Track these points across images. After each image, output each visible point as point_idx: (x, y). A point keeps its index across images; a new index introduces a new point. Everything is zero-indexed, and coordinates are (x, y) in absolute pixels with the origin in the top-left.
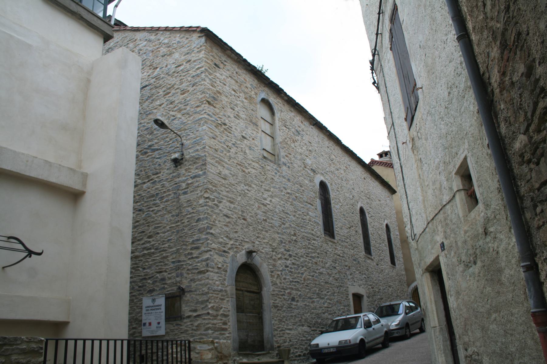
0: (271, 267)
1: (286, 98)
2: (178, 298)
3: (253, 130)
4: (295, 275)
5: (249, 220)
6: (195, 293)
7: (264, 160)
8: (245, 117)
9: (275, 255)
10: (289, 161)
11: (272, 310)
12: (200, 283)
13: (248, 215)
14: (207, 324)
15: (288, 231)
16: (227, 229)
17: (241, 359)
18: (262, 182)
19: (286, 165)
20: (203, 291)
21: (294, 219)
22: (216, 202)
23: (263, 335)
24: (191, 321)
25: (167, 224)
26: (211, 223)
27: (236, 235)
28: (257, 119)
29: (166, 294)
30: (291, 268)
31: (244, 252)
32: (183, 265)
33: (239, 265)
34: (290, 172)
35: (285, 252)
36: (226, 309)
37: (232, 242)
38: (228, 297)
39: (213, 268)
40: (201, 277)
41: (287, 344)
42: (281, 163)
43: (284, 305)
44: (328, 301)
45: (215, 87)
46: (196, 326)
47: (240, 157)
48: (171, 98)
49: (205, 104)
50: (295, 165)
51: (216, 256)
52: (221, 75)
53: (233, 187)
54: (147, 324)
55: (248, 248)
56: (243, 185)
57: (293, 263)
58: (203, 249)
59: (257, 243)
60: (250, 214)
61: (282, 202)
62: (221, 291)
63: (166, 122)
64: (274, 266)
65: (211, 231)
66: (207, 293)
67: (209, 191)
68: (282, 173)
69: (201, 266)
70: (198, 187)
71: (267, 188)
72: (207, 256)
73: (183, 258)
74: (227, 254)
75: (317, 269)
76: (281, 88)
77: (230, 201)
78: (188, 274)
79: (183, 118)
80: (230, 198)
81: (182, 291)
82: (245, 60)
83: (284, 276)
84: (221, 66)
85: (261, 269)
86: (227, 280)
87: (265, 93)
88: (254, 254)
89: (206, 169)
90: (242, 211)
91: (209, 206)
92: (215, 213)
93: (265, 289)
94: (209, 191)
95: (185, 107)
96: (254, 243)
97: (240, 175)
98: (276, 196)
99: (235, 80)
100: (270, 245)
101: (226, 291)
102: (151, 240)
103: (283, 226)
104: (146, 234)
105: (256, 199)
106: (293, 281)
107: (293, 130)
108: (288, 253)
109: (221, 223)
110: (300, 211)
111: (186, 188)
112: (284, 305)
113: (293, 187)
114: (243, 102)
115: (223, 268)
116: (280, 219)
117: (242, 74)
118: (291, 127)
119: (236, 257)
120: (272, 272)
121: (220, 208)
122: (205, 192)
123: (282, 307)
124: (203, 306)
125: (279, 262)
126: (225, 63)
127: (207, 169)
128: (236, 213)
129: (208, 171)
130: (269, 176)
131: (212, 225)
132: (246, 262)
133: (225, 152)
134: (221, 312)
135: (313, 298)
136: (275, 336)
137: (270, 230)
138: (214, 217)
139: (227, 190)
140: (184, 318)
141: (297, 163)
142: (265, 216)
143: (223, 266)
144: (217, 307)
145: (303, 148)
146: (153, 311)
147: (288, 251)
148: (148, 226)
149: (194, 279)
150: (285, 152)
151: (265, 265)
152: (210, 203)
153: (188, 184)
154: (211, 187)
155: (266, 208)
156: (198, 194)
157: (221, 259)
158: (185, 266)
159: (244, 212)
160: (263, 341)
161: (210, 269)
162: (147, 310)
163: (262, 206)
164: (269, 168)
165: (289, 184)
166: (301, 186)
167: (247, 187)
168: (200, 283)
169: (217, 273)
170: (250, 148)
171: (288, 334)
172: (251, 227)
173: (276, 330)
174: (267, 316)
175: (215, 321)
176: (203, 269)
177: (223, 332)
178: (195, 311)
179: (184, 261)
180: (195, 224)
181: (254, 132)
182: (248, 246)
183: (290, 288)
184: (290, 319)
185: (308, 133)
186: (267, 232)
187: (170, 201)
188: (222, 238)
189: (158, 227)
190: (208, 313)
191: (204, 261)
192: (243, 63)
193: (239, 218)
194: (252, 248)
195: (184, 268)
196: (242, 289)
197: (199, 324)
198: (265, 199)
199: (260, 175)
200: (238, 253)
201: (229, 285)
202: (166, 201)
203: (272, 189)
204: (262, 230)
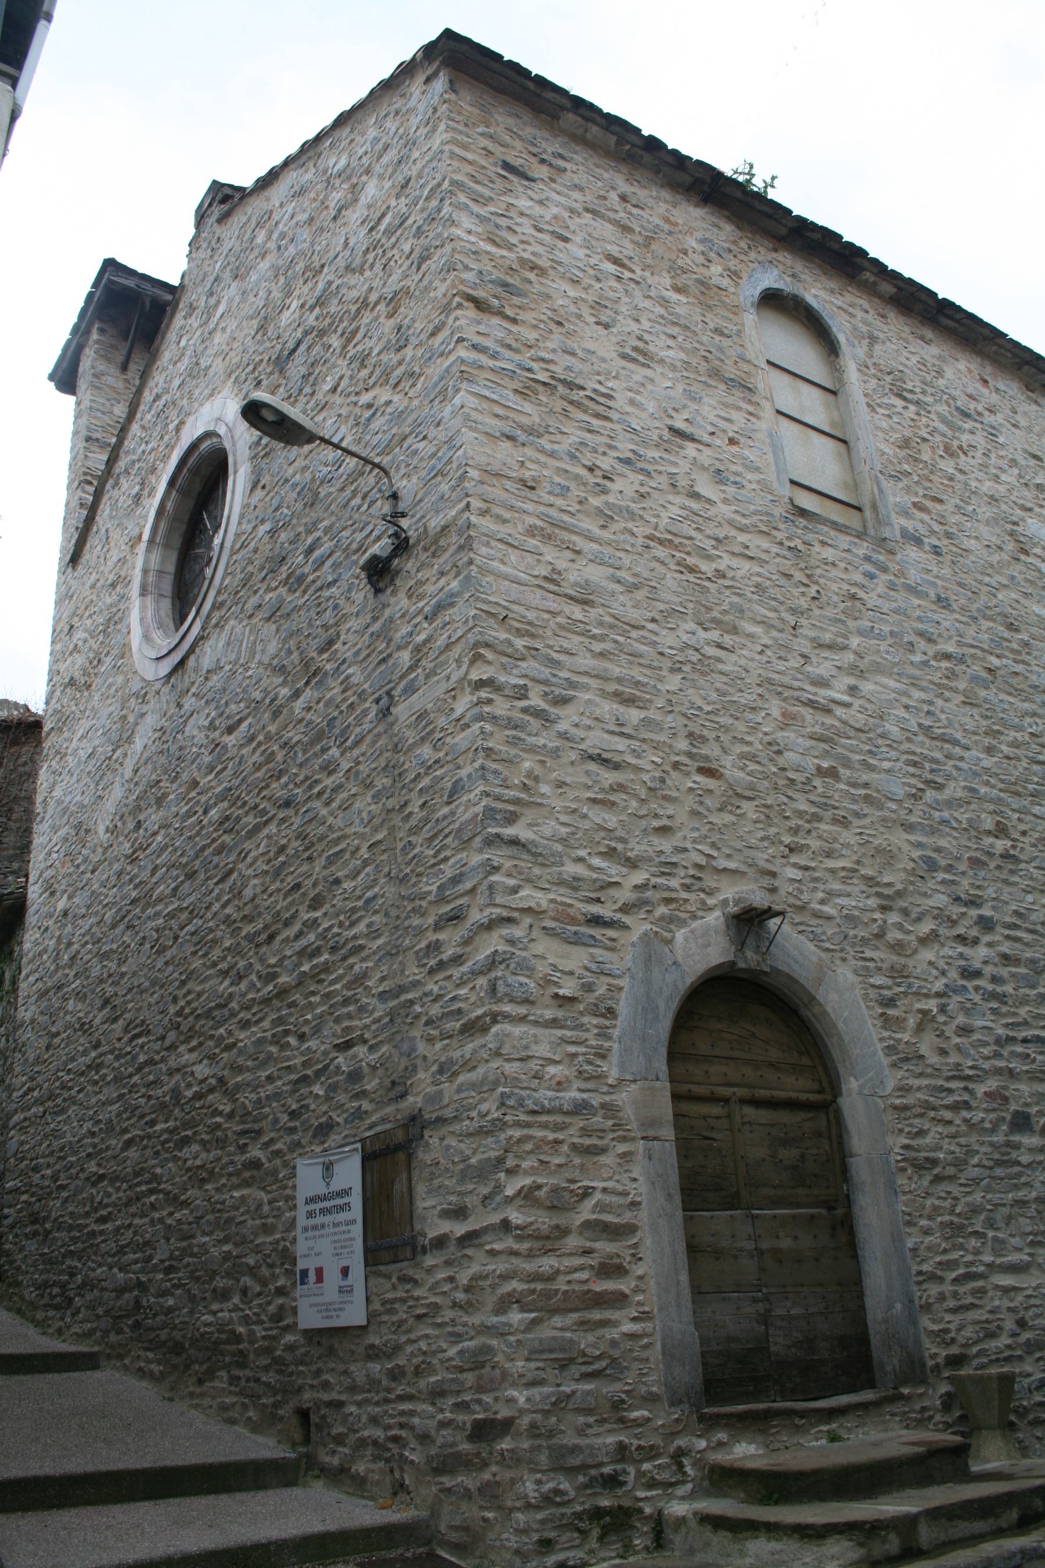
0: (878, 980)
1: (887, 288)
2: (401, 1156)
3: (726, 405)
4: (1023, 1011)
5: (732, 771)
6: (456, 1127)
7: (802, 522)
8: (682, 356)
9: (900, 927)
10: (936, 527)
11: (901, 1181)
12: (472, 1076)
13: (725, 751)
14: (505, 1277)
15: (964, 816)
16: (611, 820)
17: (721, 1444)
18: (793, 611)
19: (918, 541)
20: (483, 1116)
21: (988, 762)
22: (535, 700)
23: (862, 1308)
24: (448, 1263)
25: (362, 836)
26: (512, 793)
27: (666, 845)
28: (746, 367)
29: (362, 1141)
30: (995, 979)
31: (714, 919)
32: (411, 1002)
33: (689, 980)
34: (946, 571)
35: (956, 910)
36: (608, 1199)
37: (639, 877)
38: (624, 1139)
39: (527, 1001)
40: (474, 1052)
41: (1004, 1340)
42: (892, 532)
43: (970, 1152)
45: (511, 247)
46: (468, 1289)
47: (670, 510)
48: (360, 348)
49: (459, 306)
50: (972, 544)
51: (542, 945)
52: (541, 202)
53: (634, 634)
54: (312, 1276)
55: (737, 902)
56: (691, 626)
57: (1005, 957)
58: (476, 916)
59: (792, 873)
60: (739, 749)
61: (917, 694)
62: (580, 1108)
63: (293, 412)
64: (898, 973)
65: (509, 831)
66: (500, 1125)
67: (489, 655)
68: (901, 574)
69: (473, 999)
70: (448, 647)
71: (827, 637)
72: (493, 943)
73: (413, 972)
74: (611, 933)
76: (850, 245)
77: (616, 694)
78: (431, 1040)
79: (396, 398)
80: (619, 680)
81: (415, 1126)
82: (654, 144)
83: (961, 1019)
84: (541, 172)
85: (820, 996)
86: (614, 1058)
87: (774, 270)
88: (773, 923)
89: (471, 562)
90: (691, 735)
91: (494, 719)
92: (533, 750)
93: (851, 1085)
94: (489, 655)
95: (399, 356)
96: (773, 875)
97: (669, 582)
98: (878, 669)
99: (616, 223)
100: (869, 880)
101: (609, 1109)
102: (318, 914)
103: (930, 795)
104: (304, 894)
105: (770, 681)
106: (1011, 1040)
107: (942, 408)
108: (974, 912)
109: (572, 794)
110: (1020, 729)
111: (411, 669)
112: (970, 1152)
113: (971, 631)
114: (664, 302)
115: (591, 998)
116: (915, 764)
117: (651, 202)
118: (929, 399)
119: (669, 942)
120: (890, 1002)
121: (563, 726)
122: (472, 662)
123: (960, 1164)
124: (485, 1191)
125: (928, 954)
126: (561, 163)
127: (478, 560)
128: (656, 746)
129: (484, 571)
130: (834, 587)
131: (517, 801)
132: (733, 963)
133: (576, 491)
134: (586, 1212)
136: (927, 1308)
137: (857, 815)
138: (527, 764)
139: (598, 647)
140: (424, 1251)
141: (980, 538)
142: (826, 754)
143: (588, 988)
144: (556, 1190)
145: (1004, 477)
146: (328, 1219)
147: (973, 902)
148: (310, 858)
149: (451, 1062)
150: (908, 490)
151: (845, 974)
152: (501, 707)
153: (418, 649)
154: (503, 636)
155: (829, 721)
156: (448, 678)
157: (577, 959)
158: (418, 1009)
159: (704, 740)
160: (864, 1339)
161: (507, 1008)
162: (310, 1215)
163: (806, 712)
164: (828, 553)
165: (948, 620)
166: (1011, 627)
167: (714, 635)
168: (472, 1076)
169: (554, 1023)
170: (719, 476)
171: (1007, 1290)
172: (747, 806)
173: (933, 1277)
174: (873, 1215)
175: (547, 1264)
176: (479, 1012)
177: (597, 1315)
178: (459, 1213)
179: (416, 984)
180: (446, 810)
181: (737, 416)
182: (736, 892)
183: (998, 1071)
184: (1009, 1219)
185: (1023, 423)
186: (843, 822)
187: (368, 740)
188: (580, 860)
189: (337, 854)
190: (506, 1225)
191: (481, 973)
192: (647, 158)
193: (676, 765)
194: (759, 899)
195: (417, 1017)
196: (726, 1091)
197: (474, 1278)
198: (822, 683)
199: (783, 582)
200: (682, 923)
201: (634, 1081)
202: (357, 743)
203: (855, 642)
204: (816, 818)
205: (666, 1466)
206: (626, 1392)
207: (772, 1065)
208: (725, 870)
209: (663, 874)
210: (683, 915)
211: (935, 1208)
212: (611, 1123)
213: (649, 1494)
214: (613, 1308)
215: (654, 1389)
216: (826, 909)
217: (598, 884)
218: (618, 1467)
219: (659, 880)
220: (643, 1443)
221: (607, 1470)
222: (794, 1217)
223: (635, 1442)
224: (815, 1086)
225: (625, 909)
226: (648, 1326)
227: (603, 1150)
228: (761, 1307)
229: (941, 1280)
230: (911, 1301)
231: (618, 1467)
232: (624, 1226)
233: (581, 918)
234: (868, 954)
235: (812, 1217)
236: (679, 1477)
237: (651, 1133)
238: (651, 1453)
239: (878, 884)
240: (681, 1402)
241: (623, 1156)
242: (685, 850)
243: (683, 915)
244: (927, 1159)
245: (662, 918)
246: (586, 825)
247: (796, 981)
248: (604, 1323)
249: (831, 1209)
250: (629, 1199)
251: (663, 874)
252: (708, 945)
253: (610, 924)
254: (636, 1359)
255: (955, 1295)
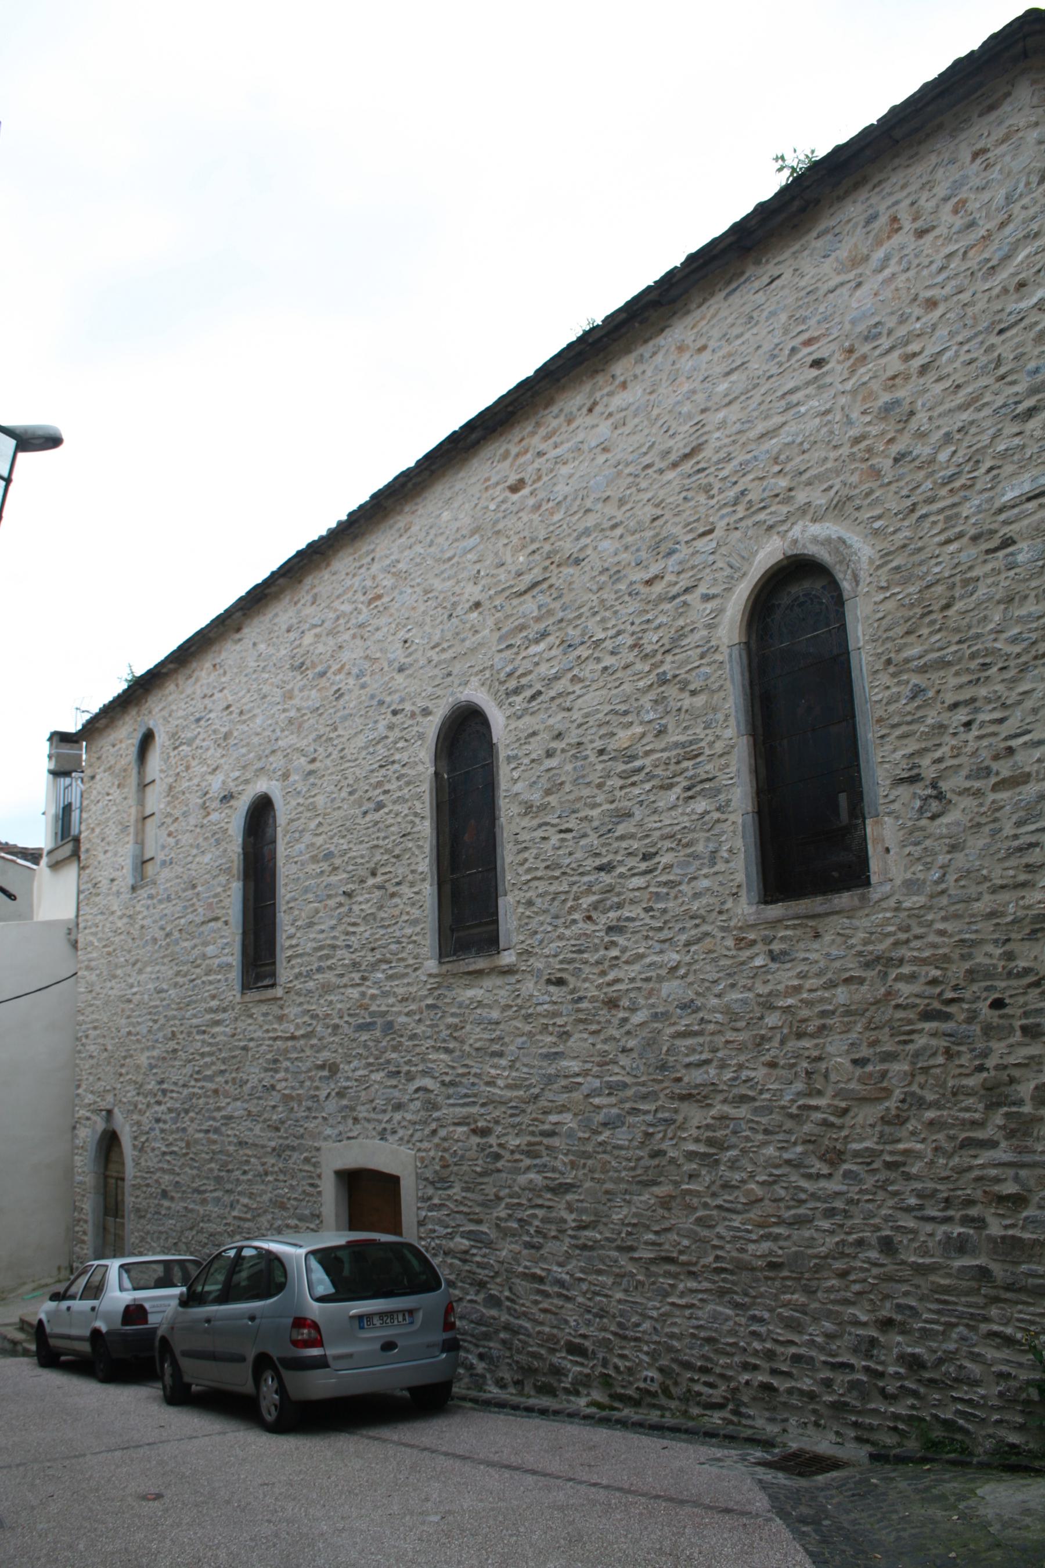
44: (245, 1200)
75: (219, 1109)
135: (205, 1191)
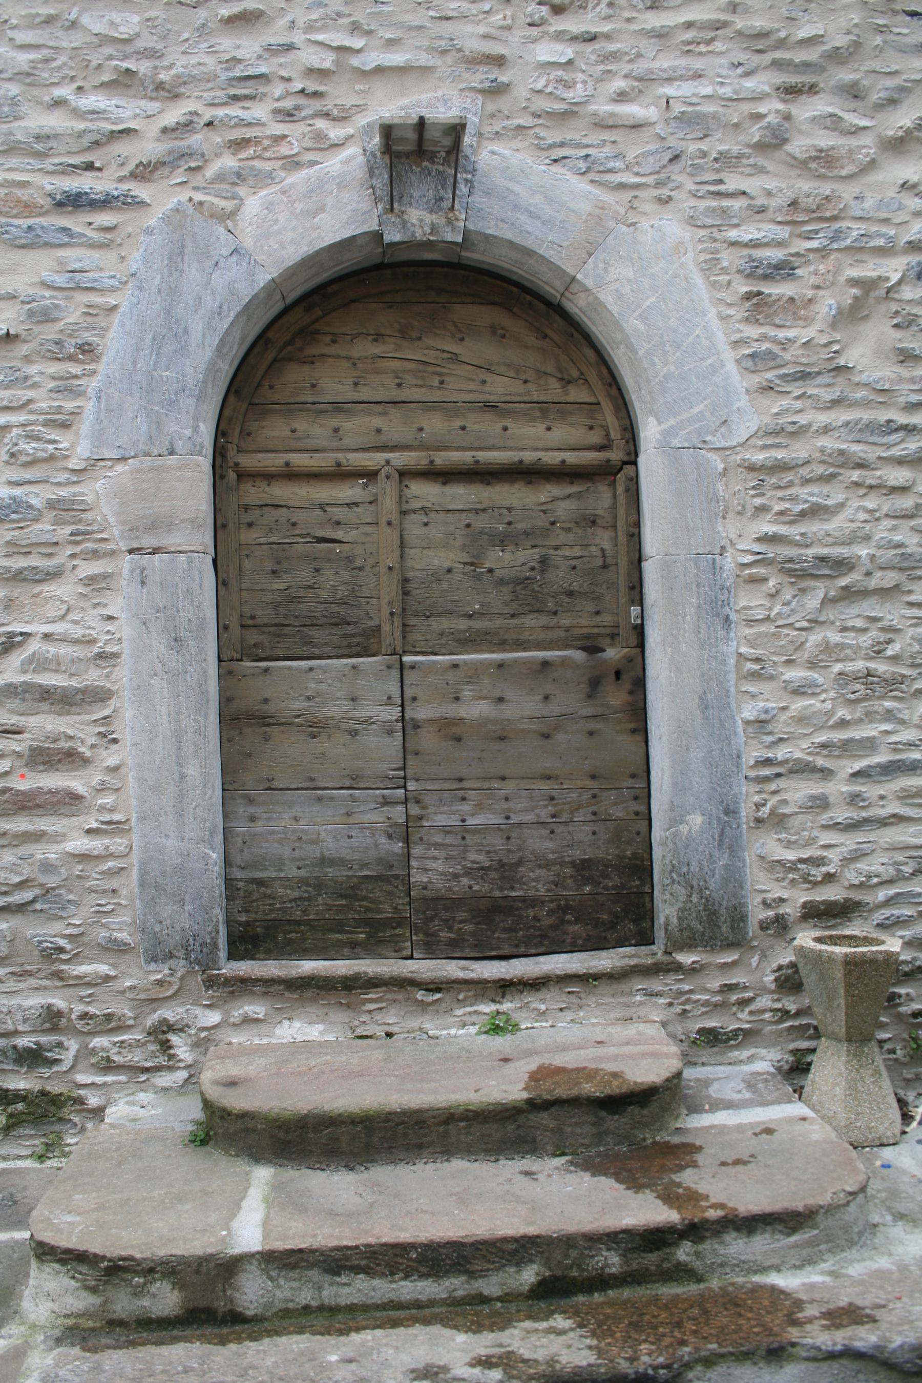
17: (248, 1021)
27: (248, 47)
33: (263, 278)
36: (52, 650)
74: (105, 218)
86: (86, 426)
96: (499, 61)
115: (51, 332)
132: (377, 236)
160: (642, 867)
188: (58, 103)
205: (139, 1044)
206: (70, 937)
207: (489, 406)
208: (379, 70)
209: (236, 98)
210: (266, 166)
211: (827, 648)
212: (68, 530)
213: (99, 1079)
214: (55, 813)
215: (119, 935)
216: (633, 110)
217: (85, 142)
218: (44, 1039)
219: (234, 111)
220: (92, 1010)
221: (23, 1042)
222: (501, 665)
223: (79, 1008)
224: (595, 438)
225: (144, 172)
226: (118, 844)
227: (53, 575)
228: (398, 813)
229: (826, 773)
230: (730, 811)
231: (44, 1039)
232: (83, 691)
233: (46, 202)
234: (733, 183)
235: (545, 664)
236: (162, 1060)
237: (148, 542)
238: (110, 1024)
239: (782, 44)
240: (171, 956)
241: (91, 580)
242: (290, 47)
243: (266, 166)
244: (823, 559)
245: (220, 178)
246: (76, 39)
247: (529, 253)
248: (38, 837)
249: (593, 649)
250: (96, 649)
251: (236, 98)
252: (322, 209)
253: (105, 203)
254: (92, 891)
255: (854, 799)
